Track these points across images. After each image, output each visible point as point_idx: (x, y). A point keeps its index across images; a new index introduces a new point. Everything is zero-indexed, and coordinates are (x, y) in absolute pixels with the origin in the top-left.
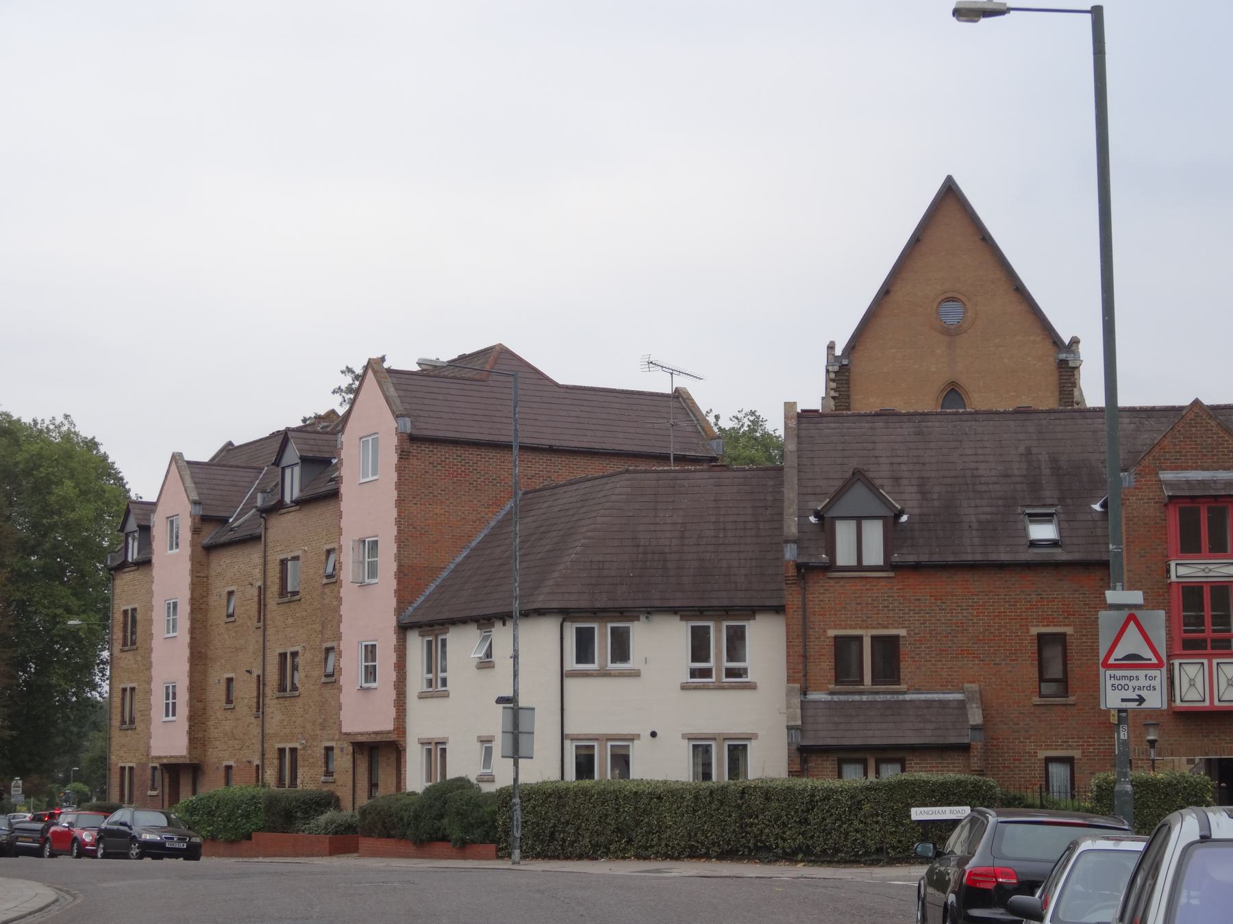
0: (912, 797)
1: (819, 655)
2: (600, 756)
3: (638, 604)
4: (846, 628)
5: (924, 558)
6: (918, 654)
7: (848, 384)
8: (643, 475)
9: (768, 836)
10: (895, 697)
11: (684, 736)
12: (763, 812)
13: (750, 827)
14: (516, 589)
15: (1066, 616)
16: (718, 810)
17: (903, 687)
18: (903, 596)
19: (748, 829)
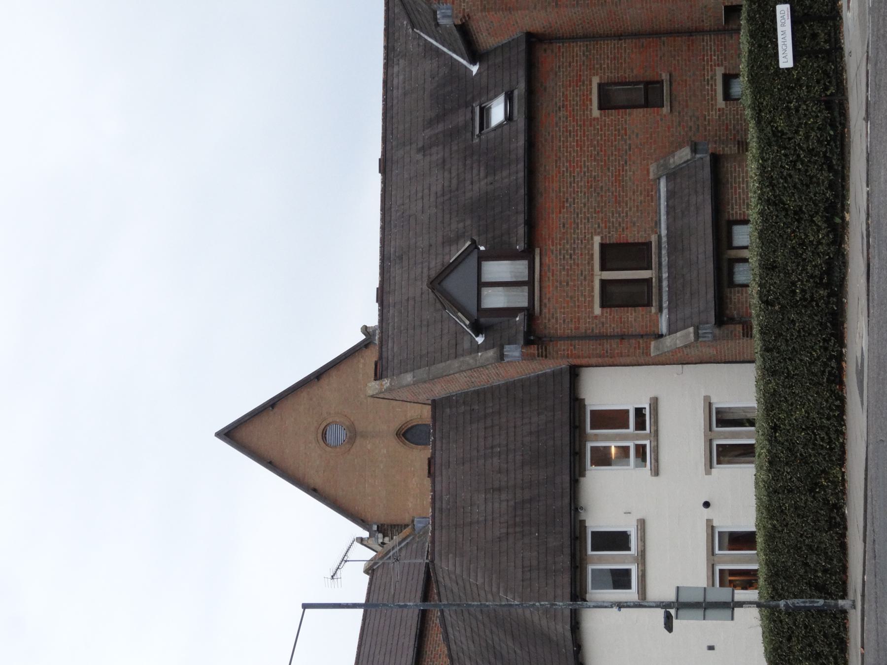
0: (767, 68)
1: (621, 323)
2: (732, 562)
3: (566, 521)
4: (593, 296)
5: (521, 218)
6: (620, 225)
7: (395, 525)
8: (437, 544)
9: (815, 266)
10: (664, 245)
11: (708, 471)
12: (788, 274)
13: (806, 293)
14: (543, 605)
15: (581, 83)
16: (787, 341)
17: (653, 238)
18: (560, 240)
19: (808, 296)
